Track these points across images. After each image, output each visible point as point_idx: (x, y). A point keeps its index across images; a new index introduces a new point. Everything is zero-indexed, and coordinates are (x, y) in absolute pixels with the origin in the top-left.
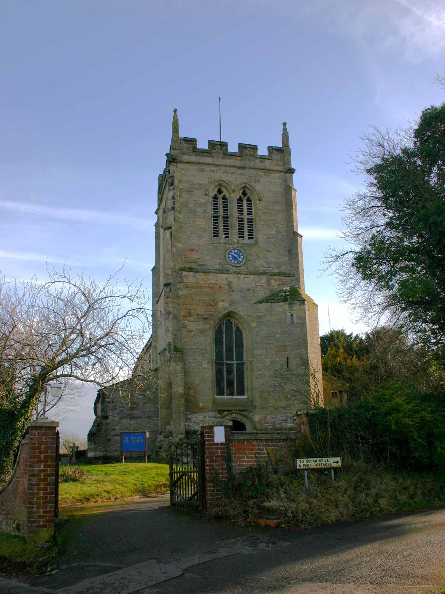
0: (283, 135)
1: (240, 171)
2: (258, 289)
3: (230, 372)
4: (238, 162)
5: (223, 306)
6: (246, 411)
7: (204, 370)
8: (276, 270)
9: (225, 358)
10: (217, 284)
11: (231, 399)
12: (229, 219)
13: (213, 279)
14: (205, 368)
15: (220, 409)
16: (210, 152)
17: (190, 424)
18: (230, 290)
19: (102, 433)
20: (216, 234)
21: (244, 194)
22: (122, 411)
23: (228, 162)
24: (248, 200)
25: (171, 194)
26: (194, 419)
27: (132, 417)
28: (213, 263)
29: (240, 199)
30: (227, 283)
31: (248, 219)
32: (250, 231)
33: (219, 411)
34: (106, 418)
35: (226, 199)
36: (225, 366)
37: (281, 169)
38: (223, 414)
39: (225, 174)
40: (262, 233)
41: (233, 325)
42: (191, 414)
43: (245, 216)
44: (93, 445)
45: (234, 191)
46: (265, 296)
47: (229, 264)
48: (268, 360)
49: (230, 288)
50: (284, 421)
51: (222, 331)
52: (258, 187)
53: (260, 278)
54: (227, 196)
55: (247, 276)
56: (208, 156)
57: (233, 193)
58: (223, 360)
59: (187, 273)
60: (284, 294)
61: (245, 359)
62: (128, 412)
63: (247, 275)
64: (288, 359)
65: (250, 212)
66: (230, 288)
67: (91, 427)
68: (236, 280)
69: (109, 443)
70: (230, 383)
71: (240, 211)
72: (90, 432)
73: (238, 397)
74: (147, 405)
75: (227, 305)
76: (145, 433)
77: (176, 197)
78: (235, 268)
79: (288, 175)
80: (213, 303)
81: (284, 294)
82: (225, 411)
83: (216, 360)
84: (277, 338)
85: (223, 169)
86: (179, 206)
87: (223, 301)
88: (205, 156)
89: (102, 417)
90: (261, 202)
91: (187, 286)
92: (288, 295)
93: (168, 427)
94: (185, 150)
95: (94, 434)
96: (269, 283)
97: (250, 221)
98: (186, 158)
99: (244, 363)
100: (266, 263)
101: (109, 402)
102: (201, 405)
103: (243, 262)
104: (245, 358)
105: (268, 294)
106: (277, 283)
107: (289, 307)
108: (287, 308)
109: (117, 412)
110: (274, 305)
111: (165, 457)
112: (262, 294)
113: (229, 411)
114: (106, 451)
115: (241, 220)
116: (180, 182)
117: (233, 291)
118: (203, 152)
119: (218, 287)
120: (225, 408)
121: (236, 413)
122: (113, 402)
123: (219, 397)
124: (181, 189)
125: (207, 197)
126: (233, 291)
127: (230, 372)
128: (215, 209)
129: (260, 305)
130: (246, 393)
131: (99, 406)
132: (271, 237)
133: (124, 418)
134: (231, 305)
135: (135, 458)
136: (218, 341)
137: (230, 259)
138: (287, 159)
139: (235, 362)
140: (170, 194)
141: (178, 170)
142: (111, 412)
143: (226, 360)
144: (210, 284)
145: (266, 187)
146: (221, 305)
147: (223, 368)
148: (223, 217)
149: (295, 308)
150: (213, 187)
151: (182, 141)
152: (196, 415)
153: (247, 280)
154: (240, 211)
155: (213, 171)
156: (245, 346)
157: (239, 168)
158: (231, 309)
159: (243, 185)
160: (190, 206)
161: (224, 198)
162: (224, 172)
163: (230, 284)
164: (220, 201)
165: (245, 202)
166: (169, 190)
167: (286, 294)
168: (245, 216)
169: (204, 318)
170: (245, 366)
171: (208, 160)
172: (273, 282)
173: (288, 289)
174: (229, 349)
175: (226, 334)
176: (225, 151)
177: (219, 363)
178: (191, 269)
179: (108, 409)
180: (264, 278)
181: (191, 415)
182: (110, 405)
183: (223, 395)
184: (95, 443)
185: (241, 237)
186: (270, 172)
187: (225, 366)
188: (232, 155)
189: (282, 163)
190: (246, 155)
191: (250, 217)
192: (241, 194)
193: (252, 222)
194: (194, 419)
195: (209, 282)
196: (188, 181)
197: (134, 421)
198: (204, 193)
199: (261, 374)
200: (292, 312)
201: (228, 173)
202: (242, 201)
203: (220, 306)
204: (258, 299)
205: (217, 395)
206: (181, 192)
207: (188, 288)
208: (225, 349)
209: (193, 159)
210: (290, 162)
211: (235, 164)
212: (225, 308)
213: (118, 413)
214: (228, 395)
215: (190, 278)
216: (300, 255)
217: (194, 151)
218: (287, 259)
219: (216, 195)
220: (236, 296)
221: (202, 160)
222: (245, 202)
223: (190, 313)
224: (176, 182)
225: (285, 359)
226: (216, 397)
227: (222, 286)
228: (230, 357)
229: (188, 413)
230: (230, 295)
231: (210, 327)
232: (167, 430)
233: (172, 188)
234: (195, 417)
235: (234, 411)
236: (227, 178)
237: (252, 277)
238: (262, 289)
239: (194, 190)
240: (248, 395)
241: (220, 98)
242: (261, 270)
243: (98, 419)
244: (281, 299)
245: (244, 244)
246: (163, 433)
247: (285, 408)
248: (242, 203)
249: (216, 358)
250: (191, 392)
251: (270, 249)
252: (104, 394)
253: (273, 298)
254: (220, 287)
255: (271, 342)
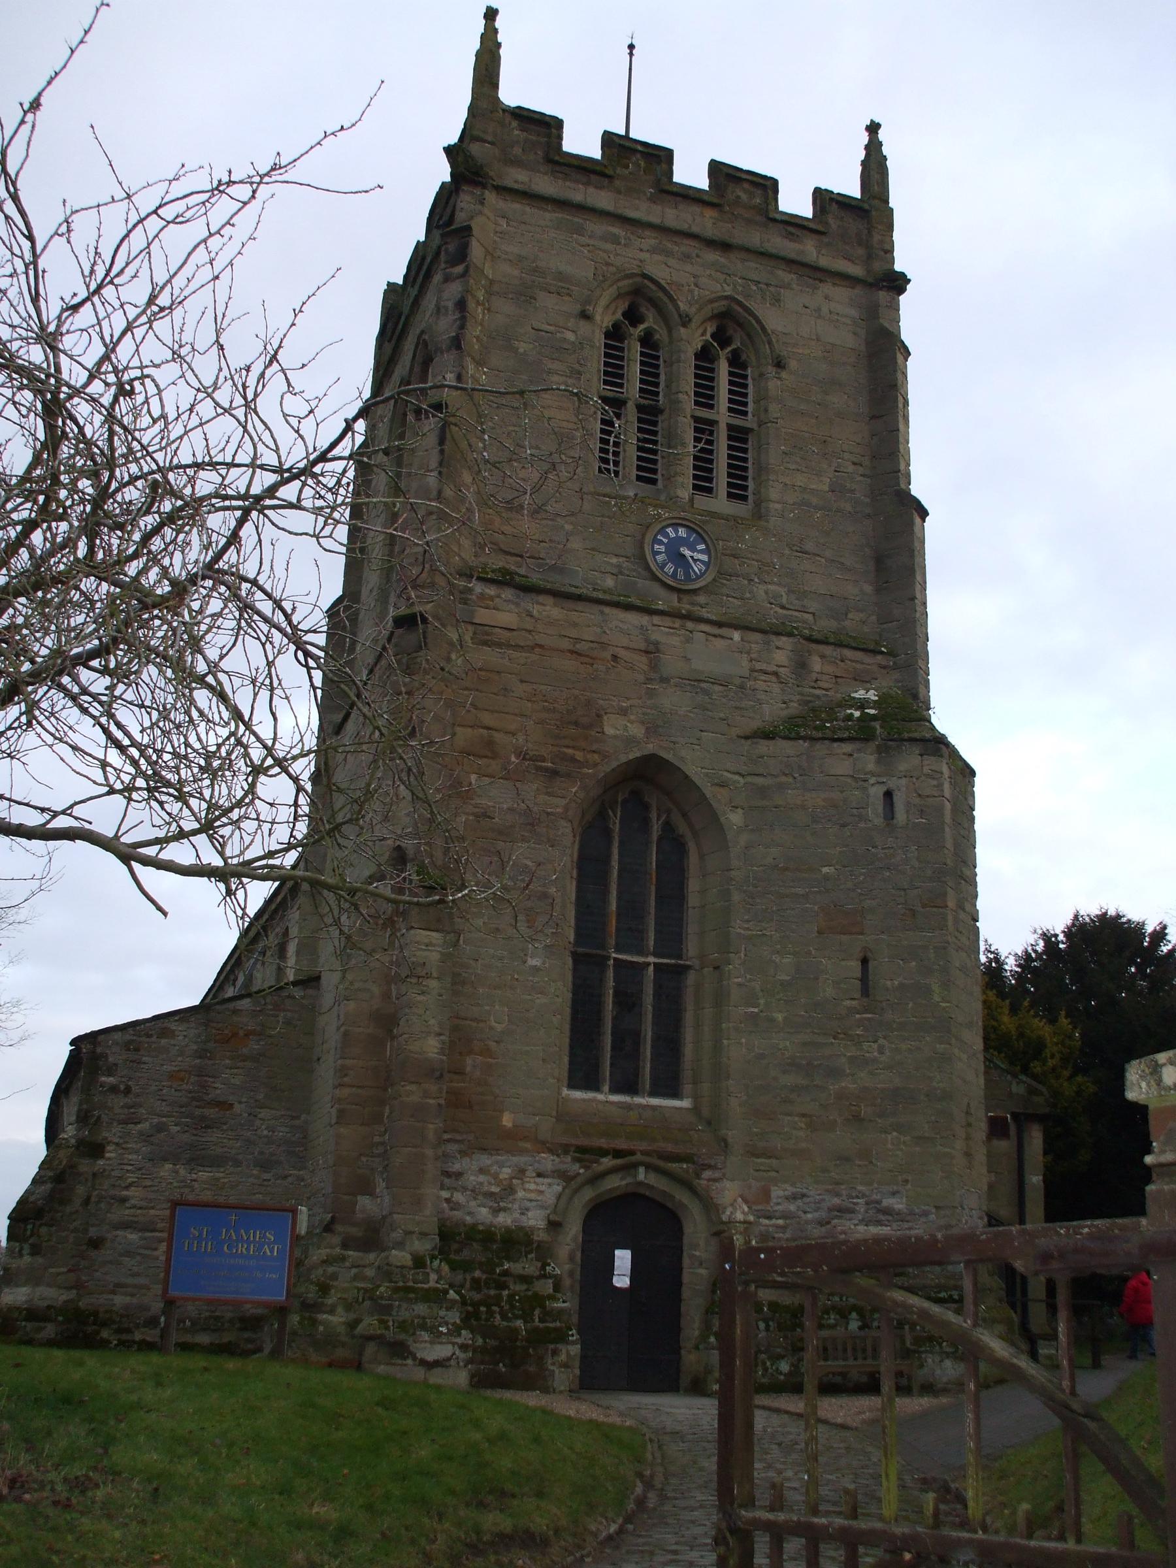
0: (864, 164)
1: (712, 256)
2: (760, 685)
3: (627, 1002)
4: (706, 222)
5: (623, 734)
6: (687, 1159)
7: (525, 982)
8: (826, 625)
9: (612, 941)
10: (604, 645)
11: (629, 1107)
12: (660, 418)
13: (588, 623)
14: (536, 969)
15: (584, 1142)
16: (609, 172)
17: (459, 1197)
18: (653, 675)
19: (68, 1209)
20: (608, 457)
21: (722, 337)
22: (160, 1128)
23: (673, 215)
24: (736, 361)
25: (454, 290)
26: (472, 1179)
27: (198, 1158)
28: (593, 565)
29: (705, 356)
30: (642, 646)
31: (730, 427)
32: (737, 471)
33: (582, 1150)
34: (94, 1149)
35: (655, 346)
36: (610, 974)
37: (856, 270)
38: (598, 1168)
39: (657, 257)
40: (787, 483)
41: (654, 815)
42: (464, 1153)
43: (722, 413)
44: (27, 1259)
45: (686, 321)
46: (785, 713)
47: (655, 578)
48: (788, 960)
49: (654, 666)
50: (842, 1211)
51: (608, 833)
52: (773, 320)
53: (767, 643)
54: (661, 334)
55: (724, 631)
56: (600, 187)
57: (684, 325)
58: (603, 946)
59: (491, 591)
60: (857, 714)
61: (691, 953)
62: (186, 1138)
63: (720, 625)
64: (865, 961)
65: (738, 405)
66: (654, 666)
67: (26, 1183)
68: (675, 641)
69: (93, 1254)
70: (626, 1043)
71: (705, 397)
72: (22, 1202)
73: (655, 1101)
74: (264, 1113)
75: (637, 731)
76: (294, 1212)
77: (471, 305)
78: (675, 597)
79: (883, 296)
80: (584, 722)
81: (857, 714)
82: (603, 1153)
83: (578, 941)
84: (827, 878)
85: (650, 240)
86: (477, 338)
87: (624, 712)
88: (587, 184)
89: (77, 1147)
90: (784, 375)
91: (485, 637)
92: (874, 718)
93: (364, 1202)
94: (517, 151)
95: (39, 1213)
96: (801, 666)
97: (738, 435)
98: (517, 177)
99: (689, 967)
100: (790, 592)
101: (114, 1089)
102: (507, 1120)
103: (709, 578)
104: (691, 948)
105: (794, 708)
106: (830, 669)
107: (878, 762)
108: (871, 766)
109: (141, 1133)
110: (821, 748)
111: (342, 1329)
112: (774, 705)
113: (618, 1154)
114: (78, 1286)
115: (704, 428)
116: (490, 254)
117: (664, 680)
118: (580, 166)
119: (607, 655)
120: (603, 1143)
121: (649, 1167)
122: (128, 1090)
123: (578, 1094)
124: (492, 282)
125: (584, 327)
126: (664, 680)
127: (627, 1002)
128: (614, 374)
129: (764, 747)
130: (687, 1088)
131: (70, 1112)
132: (814, 501)
133: (165, 1159)
134: (652, 730)
135: (193, 1324)
136: (590, 868)
137: (660, 558)
138: (882, 242)
139: (651, 959)
140: (445, 295)
141: (486, 211)
142: (117, 1129)
143: (617, 951)
144: (578, 640)
145: (805, 322)
146: (612, 727)
147: (602, 980)
148: (640, 408)
149: (903, 767)
150: (611, 292)
151: (508, 118)
152: (485, 1160)
153: (719, 643)
154: (705, 397)
155: (615, 240)
156: (693, 900)
157: (710, 243)
158: (650, 748)
159: (720, 306)
160: (523, 347)
161: (647, 340)
162: (653, 251)
163: (652, 651)
164: (634, 351)
165: (723, 369)
166: (447, 279)
167: (863, 714)
168: (722, 413)
169: (547, 769)
170: (691, 978)
171: (602, 199)
172: (816, 664)
173: (872, 695)
174: (631, 910)
175: (621, 843)
176: (664, 179)
177: (586, 964)
178: (505, 579)
179: (105, 1118)
180: (781, 654)
181: (466, 1160)
182: (118, 1102)
183: (597, 1089)
184: (36, 1251)
185: (703, 484)
186: (819, 275)
187: (610, 974)
188: (687, 194)
189: (861, 251)
190: (737, 202)
191: (738, 422)
192: (708, 337)
193: (745, 441)
194: (472, 1179)
195: (574, 633)
196: (521, 259)
197: (204, 1175)
198: (578, 307)
199: (754, 1016)
200: (892, 783)
201: (668, 253)
202: (712, 361)
203: (609, 731)
204: (756, 724)
205: (572, 1086)
206: (490, 294)
207: (485, 643)
208: (613, 906)
209: (545, 185)
210: (890, 251)
211: (695, 229)
212: (630, 741)
213: (146, 1138)
214: (615, 1090)
215: (504, 612)
216: (918, 578)
217: (549, 161)
218: (868, 589)
219: (616, 326)
220: (673, 700)
221: (578, 193)
222: (723, 369)
223: (490, 743)
224: (476, 252)
225: (855, 966)
226: (565, 1092)
227: (622, 653)
228: (632, 939)
229: (452, 1148)
230: (651, 693)
231: (566, 808)
232: (359, 1216)
233: (459, 269)
234: (482, 1171)
235: (638, 1157)
236: (659, 269)
237: (737, 636)
238: (776, 688)
239: (541, 295)
240: (696, 1098)
241: (631, 47)
242: (775, 614)
243: (62, 1154)
244: (847, 729)
245: (713, 515)
246: (339, 1228)
247: (847, 1159)
248: (712, 370)
249: (578, 934)
250: (469, 1061)
251: (809, 546)
252: (95, 1057)
253: (814, 725)
254: (615, 657)
255: (800, 891)
